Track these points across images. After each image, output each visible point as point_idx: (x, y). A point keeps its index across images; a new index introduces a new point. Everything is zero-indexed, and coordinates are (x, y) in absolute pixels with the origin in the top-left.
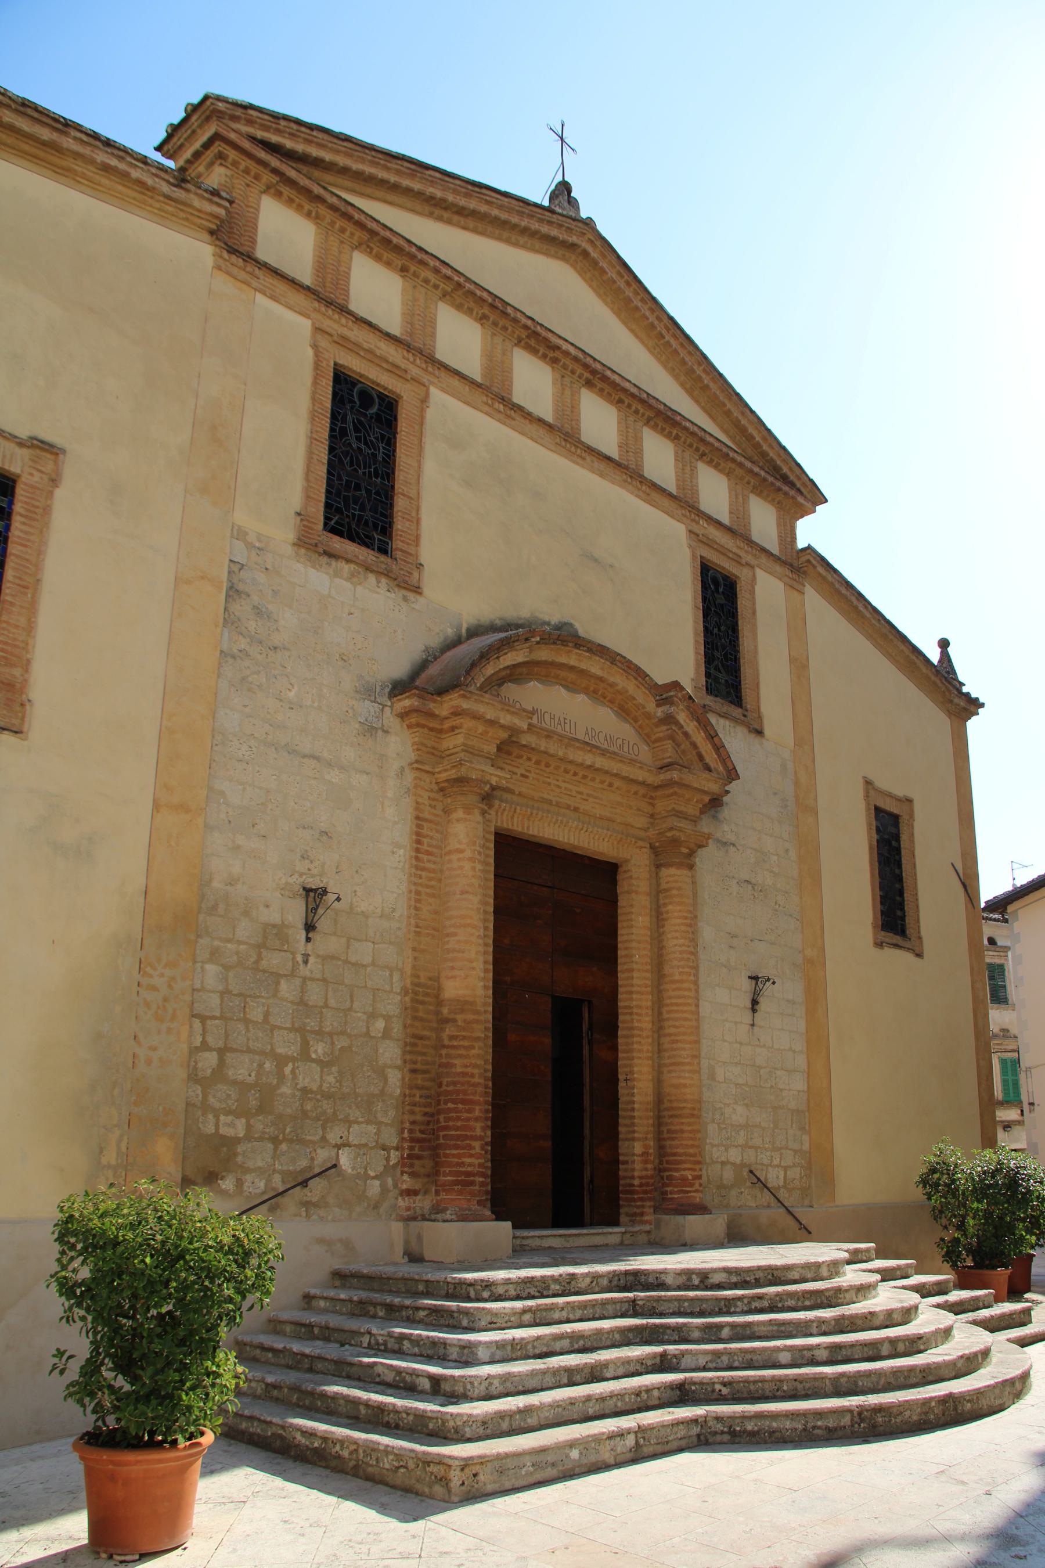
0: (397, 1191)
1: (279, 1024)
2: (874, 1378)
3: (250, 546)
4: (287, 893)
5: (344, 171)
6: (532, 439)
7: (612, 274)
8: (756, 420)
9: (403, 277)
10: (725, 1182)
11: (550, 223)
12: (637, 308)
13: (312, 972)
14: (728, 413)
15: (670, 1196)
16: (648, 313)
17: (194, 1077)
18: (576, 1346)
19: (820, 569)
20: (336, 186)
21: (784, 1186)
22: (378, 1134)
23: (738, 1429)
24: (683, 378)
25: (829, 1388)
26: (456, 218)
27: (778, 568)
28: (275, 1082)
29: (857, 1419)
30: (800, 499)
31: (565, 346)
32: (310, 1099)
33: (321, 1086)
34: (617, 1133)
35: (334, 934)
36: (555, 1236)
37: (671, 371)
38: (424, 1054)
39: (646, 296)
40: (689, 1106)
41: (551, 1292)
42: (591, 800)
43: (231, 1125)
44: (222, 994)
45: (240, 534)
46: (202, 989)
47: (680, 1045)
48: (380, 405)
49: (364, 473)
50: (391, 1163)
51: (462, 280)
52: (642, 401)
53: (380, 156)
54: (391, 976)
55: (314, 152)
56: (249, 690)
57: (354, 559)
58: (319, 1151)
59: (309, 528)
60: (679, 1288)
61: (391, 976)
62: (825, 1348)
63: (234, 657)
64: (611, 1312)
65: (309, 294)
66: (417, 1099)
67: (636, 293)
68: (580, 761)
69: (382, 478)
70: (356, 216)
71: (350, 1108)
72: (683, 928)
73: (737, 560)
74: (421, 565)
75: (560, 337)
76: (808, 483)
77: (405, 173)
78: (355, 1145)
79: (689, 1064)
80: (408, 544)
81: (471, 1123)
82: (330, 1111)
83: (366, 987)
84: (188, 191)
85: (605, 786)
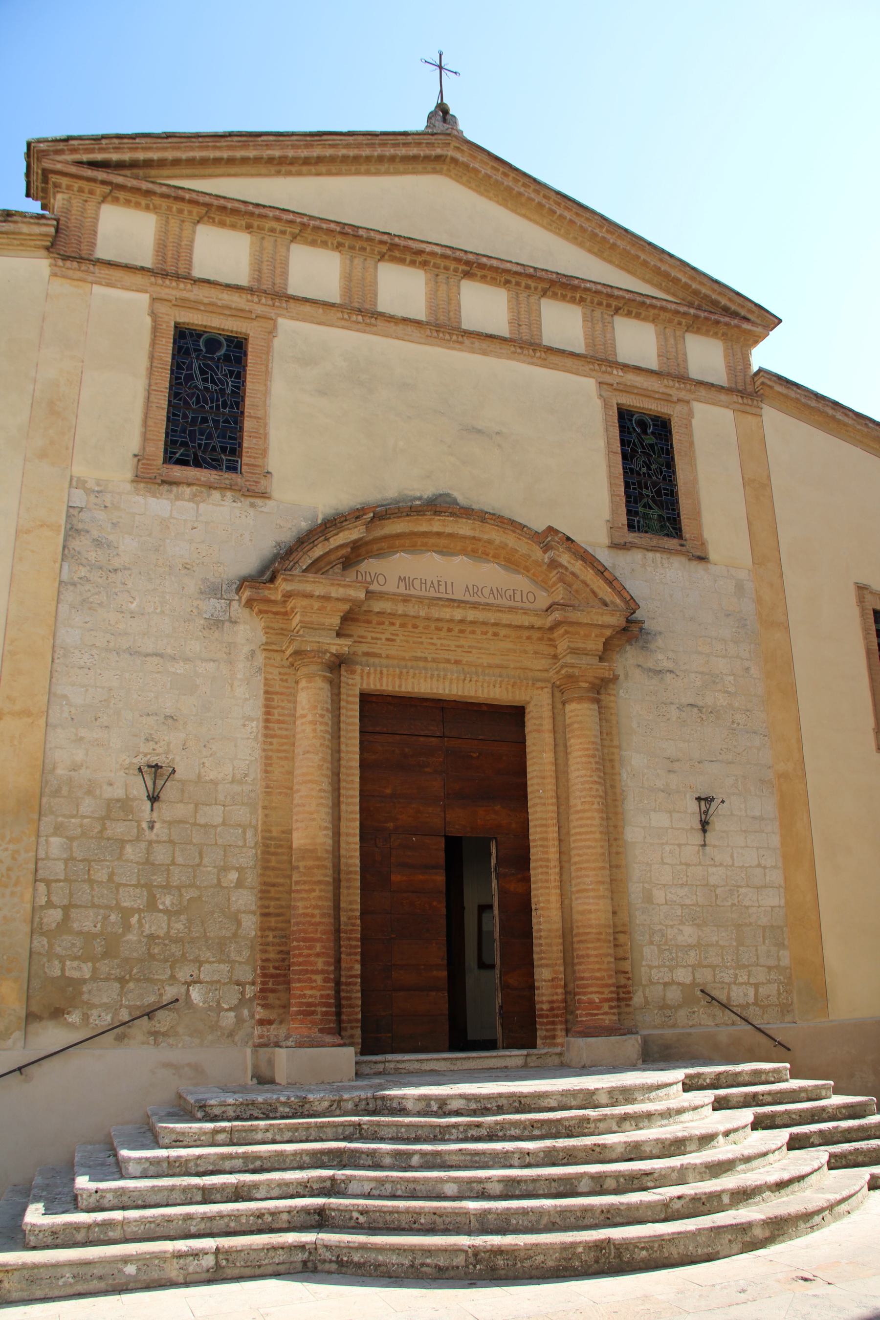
0: (253, 1021)
1: (124, 882)
2: (533, 1218)
3: (89, 492)
4: (131, 772)
5: (176, 162)
6: (397, 338)
7: (486, 170)
8: (678, 263)
9: (250, 233)
10: (669, 1002)
11: (405, 145)
12: (520, 194)
13: (158, 836)
14: (645, 264)
15: (580, 1019)
16: (533, 195)
17: (36, 929)
18: (251, 1166)
19: (778, 388)
20: (162, 177)
21: (756, 1003)
22: (231, 971)
23: (345, 1259)
24: (588, 244)
25: (474, 1224)
26: (305, 169)
27: (723, 397)
28: (121, 931)
29: (472, 1260)
30: (746, 326)
31: (429, 248)
32: (158, 944)
33: (168, 932)
34: (532, 960)
35: (181, 801)
36: (437, 1060)
37: (575, 241)
38: (278, 899)
39: (527, 180)
40: (594, 931)
41: (278, 1114)
42: (474, 651)
43: (79, 968)
44: (66, 861)
45: (79, 483)
46: (47, 858)
47: (584, 872)
48: (228, 346)
49: (211, 408)
50: (247, 997)
51: (305, 220)
52: (530, 276)
53: (207, 139)
54: (244, 832)
55: (141, 156)
56: (90, 609)
57: (195, 482)
58: (167, 988)
59: (148, 464)
60: (419, 1114)
61: (244, 832)
62: (499, 1181)
63: (74, 584)
64: (330, 1136)
65: (144, 272)
66: (271, 939)
67: (516, 181)
68: (448, 617)
69: (232, 407)
70: (187, 196)
71: (200, 949)
72: (584, 759)
73: (667, 399)
74: (268, 473)
75: (422, 242)
76: (754, 308)
77: (236, 147)
78: (207, 982)
79: (593, 890)
80: (255, 458)
81: (312, 959)
82: (178, 954)
83: (216, 844)
84: (15, 222)
85: (489, 635)
